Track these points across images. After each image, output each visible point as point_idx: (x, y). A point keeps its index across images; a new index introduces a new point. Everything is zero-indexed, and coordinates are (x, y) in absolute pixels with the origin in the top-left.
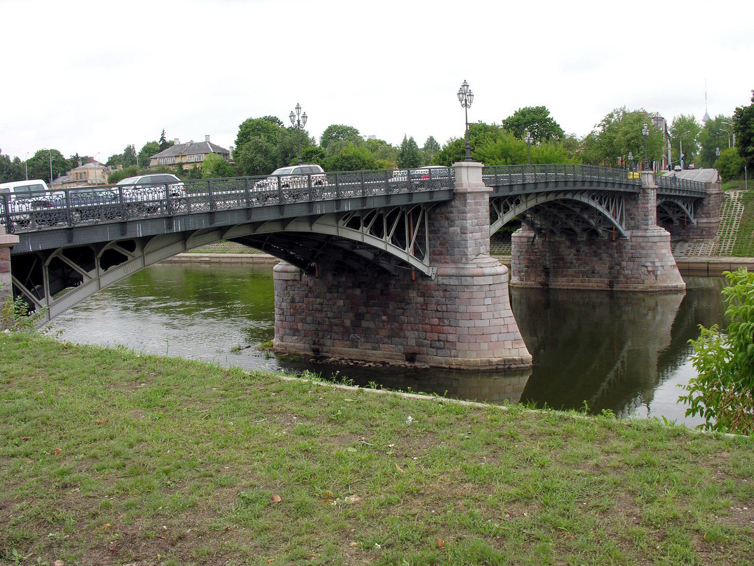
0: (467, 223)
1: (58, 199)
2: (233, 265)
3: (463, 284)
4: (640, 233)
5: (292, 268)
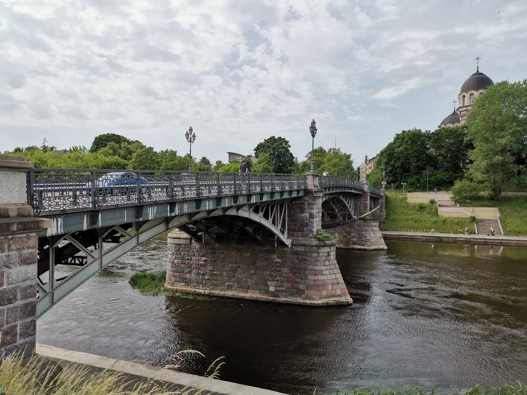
1: (112, 179)
5: (185, 235)
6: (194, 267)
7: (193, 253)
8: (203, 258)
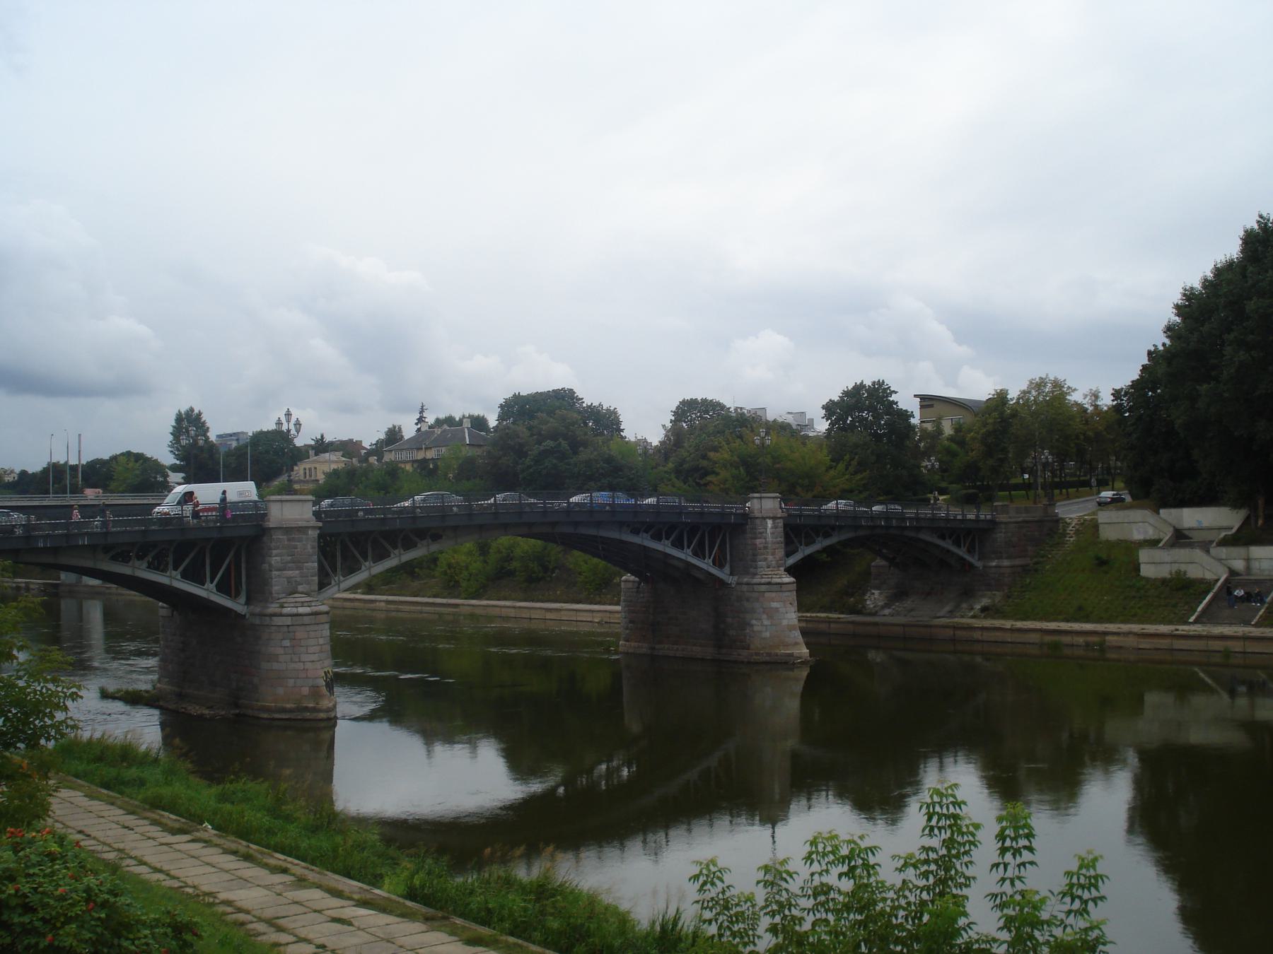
2: (579, 623)
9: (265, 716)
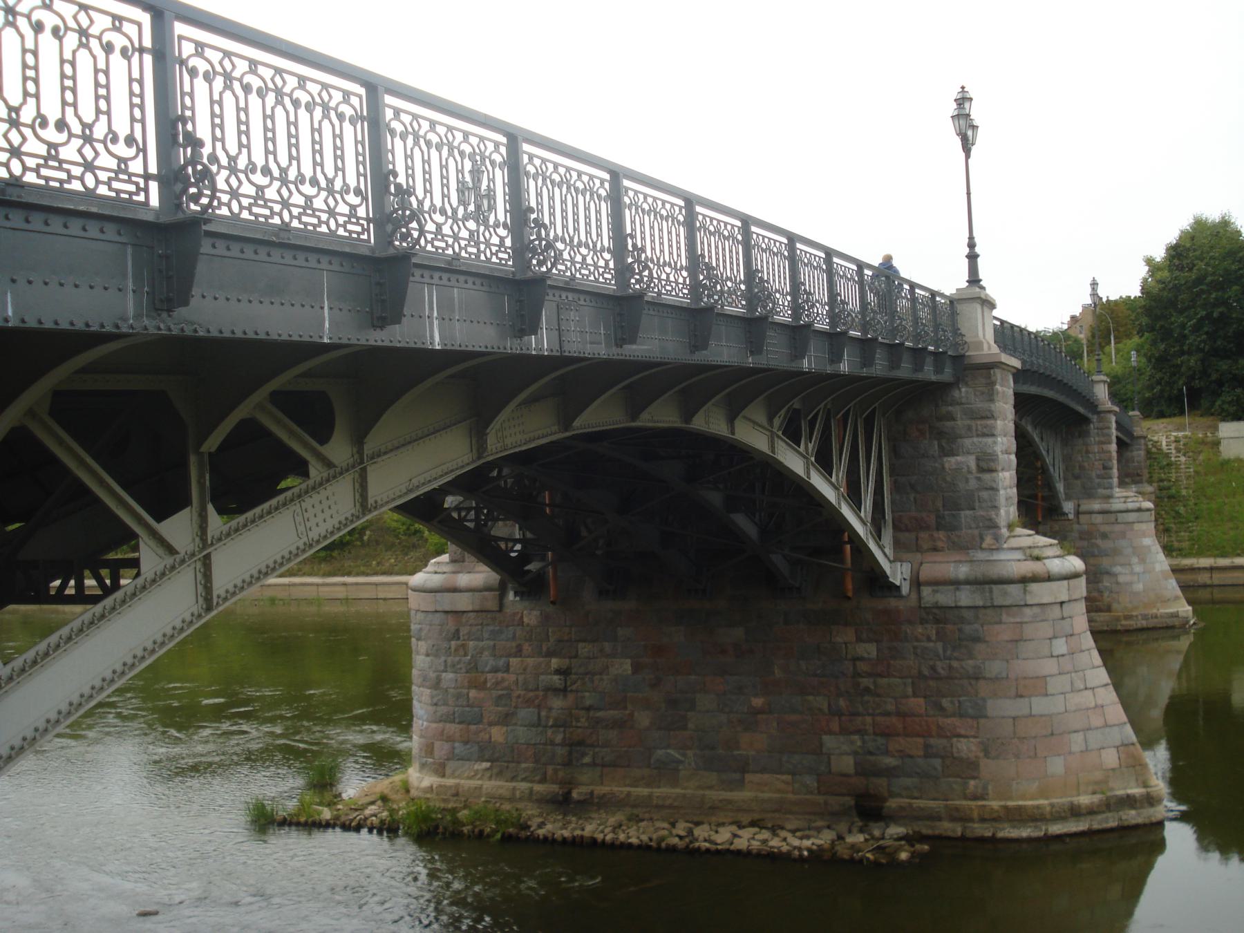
0: (995, 443)
3: (995, 604)
4: (1096, 506)
6: (519, 697)
7: (514, 644)
8: (555, 662)
9: (1025, 833)
